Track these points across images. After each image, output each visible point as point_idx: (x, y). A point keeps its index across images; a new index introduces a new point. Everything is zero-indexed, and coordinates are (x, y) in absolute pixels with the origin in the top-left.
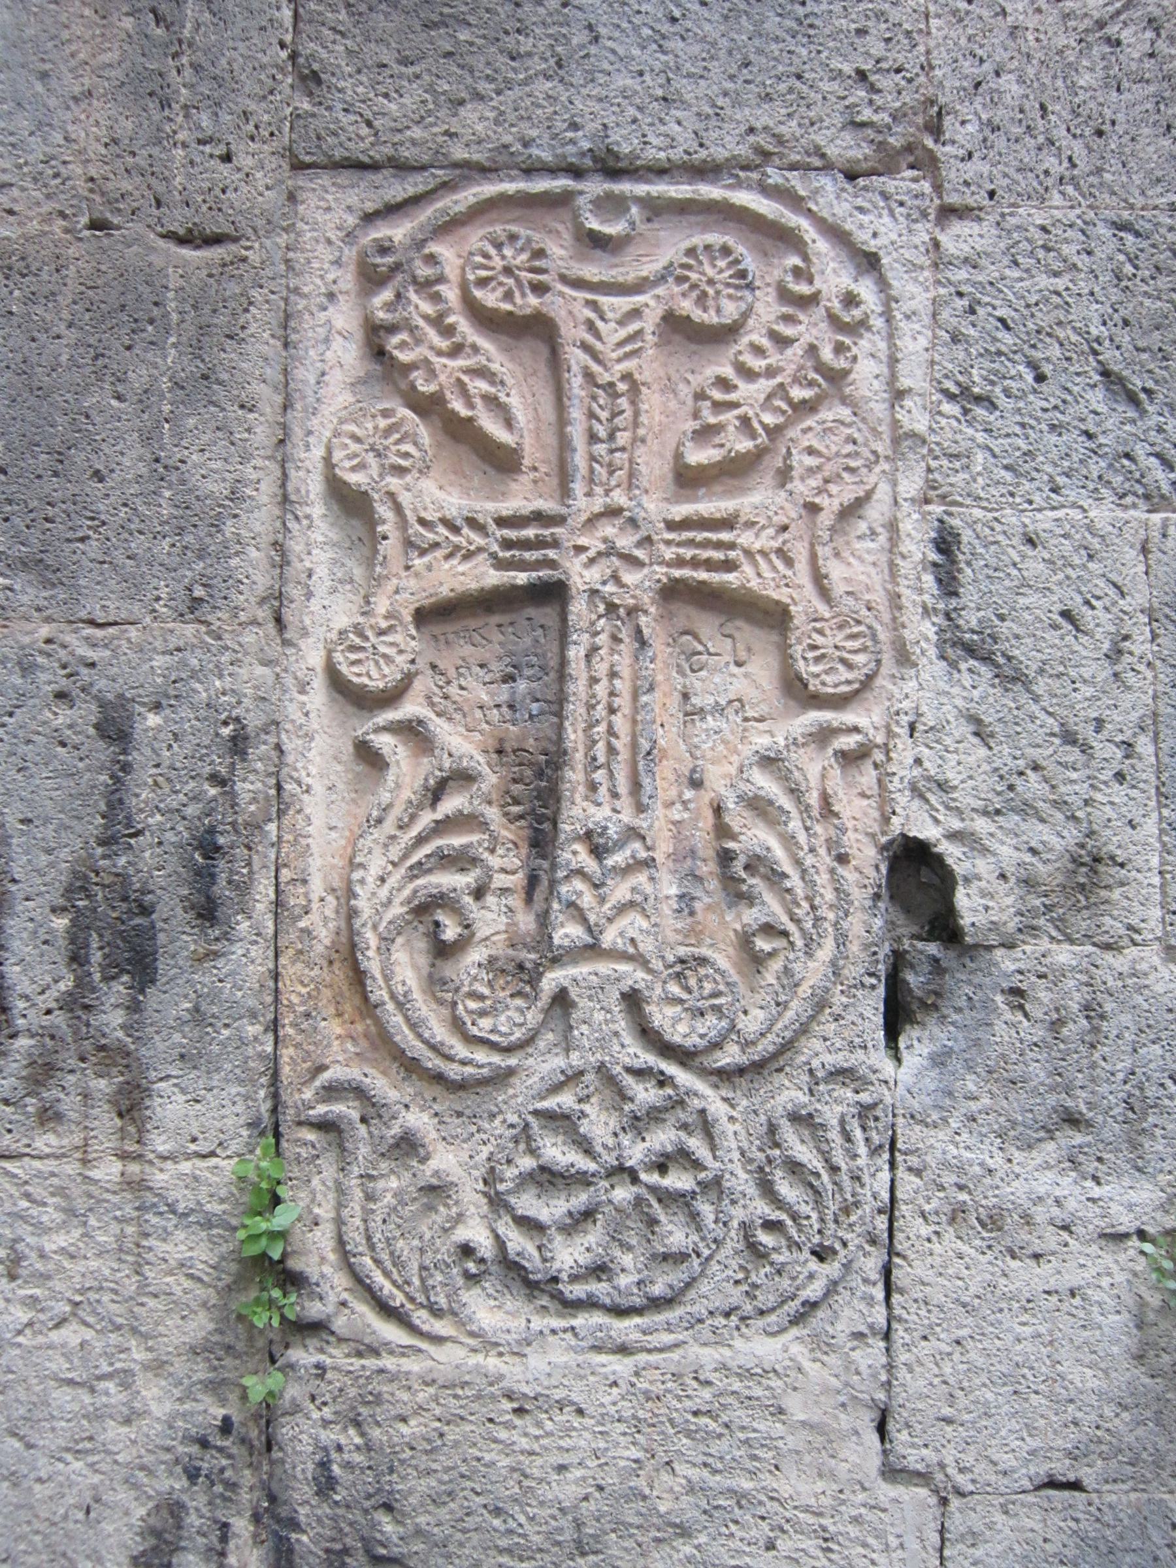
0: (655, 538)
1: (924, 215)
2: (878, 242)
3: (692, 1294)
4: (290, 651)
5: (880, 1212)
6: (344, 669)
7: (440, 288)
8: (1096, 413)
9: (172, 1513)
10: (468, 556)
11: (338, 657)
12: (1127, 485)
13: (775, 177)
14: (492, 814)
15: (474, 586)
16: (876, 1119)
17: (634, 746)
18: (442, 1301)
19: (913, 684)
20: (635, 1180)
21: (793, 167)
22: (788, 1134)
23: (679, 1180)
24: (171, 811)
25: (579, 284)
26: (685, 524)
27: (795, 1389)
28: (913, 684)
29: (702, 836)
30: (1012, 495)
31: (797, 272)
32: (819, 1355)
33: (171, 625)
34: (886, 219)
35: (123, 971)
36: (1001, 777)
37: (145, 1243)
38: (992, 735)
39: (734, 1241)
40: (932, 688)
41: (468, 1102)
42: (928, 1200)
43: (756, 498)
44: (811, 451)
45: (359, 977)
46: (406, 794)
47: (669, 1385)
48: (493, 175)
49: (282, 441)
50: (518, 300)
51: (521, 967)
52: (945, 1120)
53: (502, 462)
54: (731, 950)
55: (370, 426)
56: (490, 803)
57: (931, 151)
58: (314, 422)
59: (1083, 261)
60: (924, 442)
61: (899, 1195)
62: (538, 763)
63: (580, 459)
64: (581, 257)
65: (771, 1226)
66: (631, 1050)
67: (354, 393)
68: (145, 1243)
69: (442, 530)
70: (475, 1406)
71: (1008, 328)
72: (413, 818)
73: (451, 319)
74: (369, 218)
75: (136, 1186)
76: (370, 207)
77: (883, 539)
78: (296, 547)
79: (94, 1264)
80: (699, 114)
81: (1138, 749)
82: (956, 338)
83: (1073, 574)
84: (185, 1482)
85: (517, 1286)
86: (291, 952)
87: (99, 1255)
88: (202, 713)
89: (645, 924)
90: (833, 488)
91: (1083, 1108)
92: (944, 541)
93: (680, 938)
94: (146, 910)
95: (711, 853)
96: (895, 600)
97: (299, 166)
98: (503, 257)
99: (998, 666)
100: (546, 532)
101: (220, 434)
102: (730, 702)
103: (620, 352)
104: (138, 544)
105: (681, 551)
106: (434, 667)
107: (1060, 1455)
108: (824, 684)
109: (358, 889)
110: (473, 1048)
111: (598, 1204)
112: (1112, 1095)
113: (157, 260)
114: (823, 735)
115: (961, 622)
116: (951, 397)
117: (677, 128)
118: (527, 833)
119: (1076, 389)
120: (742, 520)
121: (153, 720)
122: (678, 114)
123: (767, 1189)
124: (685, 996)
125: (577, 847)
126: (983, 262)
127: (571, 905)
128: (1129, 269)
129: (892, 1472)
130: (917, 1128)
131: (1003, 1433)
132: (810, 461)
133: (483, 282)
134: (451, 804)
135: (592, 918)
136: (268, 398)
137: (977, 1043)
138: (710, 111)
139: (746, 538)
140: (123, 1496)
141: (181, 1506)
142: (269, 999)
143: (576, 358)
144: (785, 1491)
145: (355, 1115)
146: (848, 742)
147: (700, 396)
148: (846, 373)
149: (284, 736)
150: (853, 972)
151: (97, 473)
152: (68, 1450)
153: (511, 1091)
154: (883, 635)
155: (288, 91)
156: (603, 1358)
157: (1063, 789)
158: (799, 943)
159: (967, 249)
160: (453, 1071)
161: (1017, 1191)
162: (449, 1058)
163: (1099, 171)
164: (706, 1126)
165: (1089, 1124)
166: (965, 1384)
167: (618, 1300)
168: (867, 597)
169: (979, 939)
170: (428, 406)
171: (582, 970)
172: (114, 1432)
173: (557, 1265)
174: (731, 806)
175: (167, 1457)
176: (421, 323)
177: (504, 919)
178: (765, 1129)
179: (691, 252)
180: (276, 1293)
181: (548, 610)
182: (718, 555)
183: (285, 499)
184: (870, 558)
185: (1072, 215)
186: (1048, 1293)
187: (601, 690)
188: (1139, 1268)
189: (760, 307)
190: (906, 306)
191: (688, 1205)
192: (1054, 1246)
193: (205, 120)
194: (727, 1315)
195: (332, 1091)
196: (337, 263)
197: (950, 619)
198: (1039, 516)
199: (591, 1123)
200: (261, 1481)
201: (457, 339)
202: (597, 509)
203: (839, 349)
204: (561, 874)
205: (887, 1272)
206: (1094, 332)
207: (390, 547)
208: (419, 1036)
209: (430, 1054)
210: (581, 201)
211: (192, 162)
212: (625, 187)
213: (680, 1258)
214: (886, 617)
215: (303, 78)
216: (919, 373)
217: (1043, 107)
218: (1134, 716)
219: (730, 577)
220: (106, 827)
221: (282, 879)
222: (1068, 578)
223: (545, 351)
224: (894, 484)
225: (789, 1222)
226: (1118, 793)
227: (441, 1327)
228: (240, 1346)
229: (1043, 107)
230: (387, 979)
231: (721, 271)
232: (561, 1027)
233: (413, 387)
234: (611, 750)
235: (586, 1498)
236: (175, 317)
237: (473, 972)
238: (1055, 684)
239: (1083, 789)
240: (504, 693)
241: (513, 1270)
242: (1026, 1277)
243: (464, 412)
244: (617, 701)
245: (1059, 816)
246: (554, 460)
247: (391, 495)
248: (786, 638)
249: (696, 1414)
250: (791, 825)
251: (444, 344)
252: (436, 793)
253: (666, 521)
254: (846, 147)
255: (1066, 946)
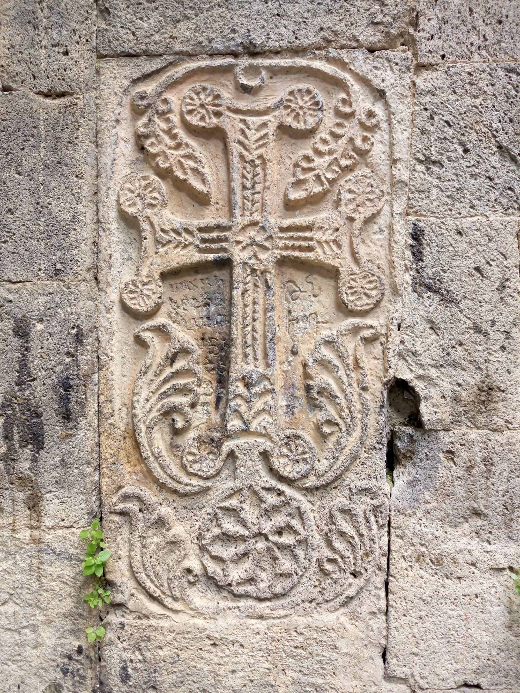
0: (274, 236)
1: (408, 69)
2: (385, 84)
3: (294, 592)
4: (102, 293)
5: (383, 555)
6: (127, 302)
7: (169, 115)
8: (494, 168)
9: (56, 689)
10: (185, 246)
11: (125, 296)
12: (509, 204)
13: (333, 53)
14: (199, 368)
15: (188, 261)
16: (381, 512)
17: (265, 336)
18: (178, 594)
19: (400, 304)
20: (267, 539)
21: (342, 47)
22: (339, 518)
23: (287, 539)
24: (49, 369)
25: (237, 111)
26: (289, 229)
27: (342, 638)
28: (400, 304)
29: (298, 378)
30: (451, 210)
31: (344, 101)
32: (354, 622)
33: (46, 282)
34: (389, 72)
35: (28, 443)
36: (443, 349)
37: (42, 567)
38: (439, 329)
39: (314, 567)
40: (409, 306)
41: (189, 502)
42: (406, 551)
43: (323, 215)
44: (350, 191)
45: (137, 445)
46: (158, 360)
47: (283, 634)
48: (195, 58)
49: (96, 193)
50: (208, 121)
51: (212, 440)
52: (414, 513)
53: (201, 200)
54: (311, 431)
55: (137, 185)
56: (198, 363)
57: (412, 35)
58: (111, 183)
59: (490, 90)
60: (407, 185)
61: (392, 548)
62: (220, 344)
63: (238, 198)
64: (238, 98)
65: (331, 561)
66: (264, 479)
67: (131, 168)
68: (42, 567)
69: (172, 234)
70: (193, 643)
71: (450, 126)
72: (161, 371)
73: (175, 131)
74: (135, 82)
75: (37, 541)
76: (135, 76)
77: (386, 233)
78: (103, 244)
79: (19, 576)
80: (295, 22)
81: (513, 335)
82: (423, 132)
83: (481, 249)
84: (62, 675)
85: (212, 587)
86: (105, 434)
87: (21, 572)
88: (62, 323)
89: (270, 420)
90: (361, 209)
91: (482, 508)
92: (416, 234)
93: (287, 425)
94: (39, 415)
95: (301, 386)
96: (391, 264)
97: (101, 57)
98: (200, 99)
99: (442, 295)
100: (222, 234)
101: (67, 190)
102: (311, 314)
103: (257, 144)
104: (30, 244)
105: (287, 242)
106: (171, 299)
107: (470, 672)
108: (356, 305)
109: (136, 405)
110: (191, 477)
111: (250, 550)
112: (497, 502)
113: (35, 106)
114: (355, 330)
115: (424, 274)
116: (421, 162)
117: (284, 30)
118: (215, 377)
119: (484, 156)
120: (316, 226)
121: (39, 327)
122: (285, 22)
123: (329, 543)
124: (289, 454)
125: (239, 384)
126: (438, 92)
127: (236, 411)
128: (513, 92)
129: (389, 677)
130: (401, 517)
131: (442, 661)
132: (350, 196)
133: (190, 112)
134: (179, 365)
135: (245, 417)
136: (89, 172)
137: (430, 476)
138: (301, 20)
139: (318, 235)
140: (34, 681)
141: (61, 686)
142: (96, 456)
143: (235, 148)
144: (338, 685)
145: (137, 509)
146: (368, 333)
147: (296, 165)
148: (368, 151)
149: (100, 334)
150: (369, 442)
151: (10, 210)
152: (9, 660)
153: (209, 497)
154: (385, 281)
155: (95, 18)
156: (252, 621)
157: (474, 355)
158: (344, 429)
159: (430, 85)
160: (181, 489)
161: (449, 547)
162: (180, 483)
163: (499, 42)
164: (300, 514)
165: (485, 516)
166: (424, 638)
167: (259, 595)
168: (378, 262)
169: (432, 427)
170: (165, 174)
171: (241, 441)
172: (29, 652)
173: (230, 578)
174: (310, 364)
175: (54, 664)
176: (161, 133)
177: (205, 417)
178: (328, 515)
179: (291, 93)
180: (101, 591)
181: (224, 272)
182: (304, 244)
183: (98, 221)
184: (380, 243)
185: (484, 66)
186: (465, 596)
187: (249, 310)
188: (509, 585)
189: (326, 120)
190: (398, 117)
191: (292, 551)
192: (467, 574)
193: (55, 34)
194: (311, 602)
195: (126, 498)
196: (120, 104)
197: (419, 273)
198: (464, 220)
199: (246, 513)
200: (96, 675)
201: (178, 141)
202: (246, 223)
203: (365, 139)
204: (231, 396)
205: (387, 583)
206: (495, 126)
207: (149, 243)
208: (166, 472)
209: (171, 481)
210: (237, 69)
211: (49, 56)
212: (259, 61)
213: (289, 575)
214: (387, 272)
215: (101, 11)
216: (404, 150)
217: (471, 10)
218: (511, 318)
219: (311, 255)
220: (19, 377)
221: (101, 401)
222: (478, 251)
223: (221, 145)
224: (392, 206)
225: (340, 560)
226: (502, 356)
227: (177, 606)
228: (85, 614)
229: (471, 10)
230: (150, 446)
231: (306, 102)
232: (232, 467)
233: (158, 165)
234: (254, 339)
235: (245, 686)
236: (43, 133)
237: (190, 442)
238: (471, 303)
239: (484, 355)
240: (204, 311)
241: (210, 579)
242: (454, 588)
243: (182, 177)
244: (257, 315)
245: (472, 367)
246: (226, 199)
247: (148, 218)
248: (337, 283)
249: (296, 648)
250: (340, 373)
251: (172, 143)
252: (172, 359)
253: (279, 228)
254: (369, 36)
255: (475, 430)
